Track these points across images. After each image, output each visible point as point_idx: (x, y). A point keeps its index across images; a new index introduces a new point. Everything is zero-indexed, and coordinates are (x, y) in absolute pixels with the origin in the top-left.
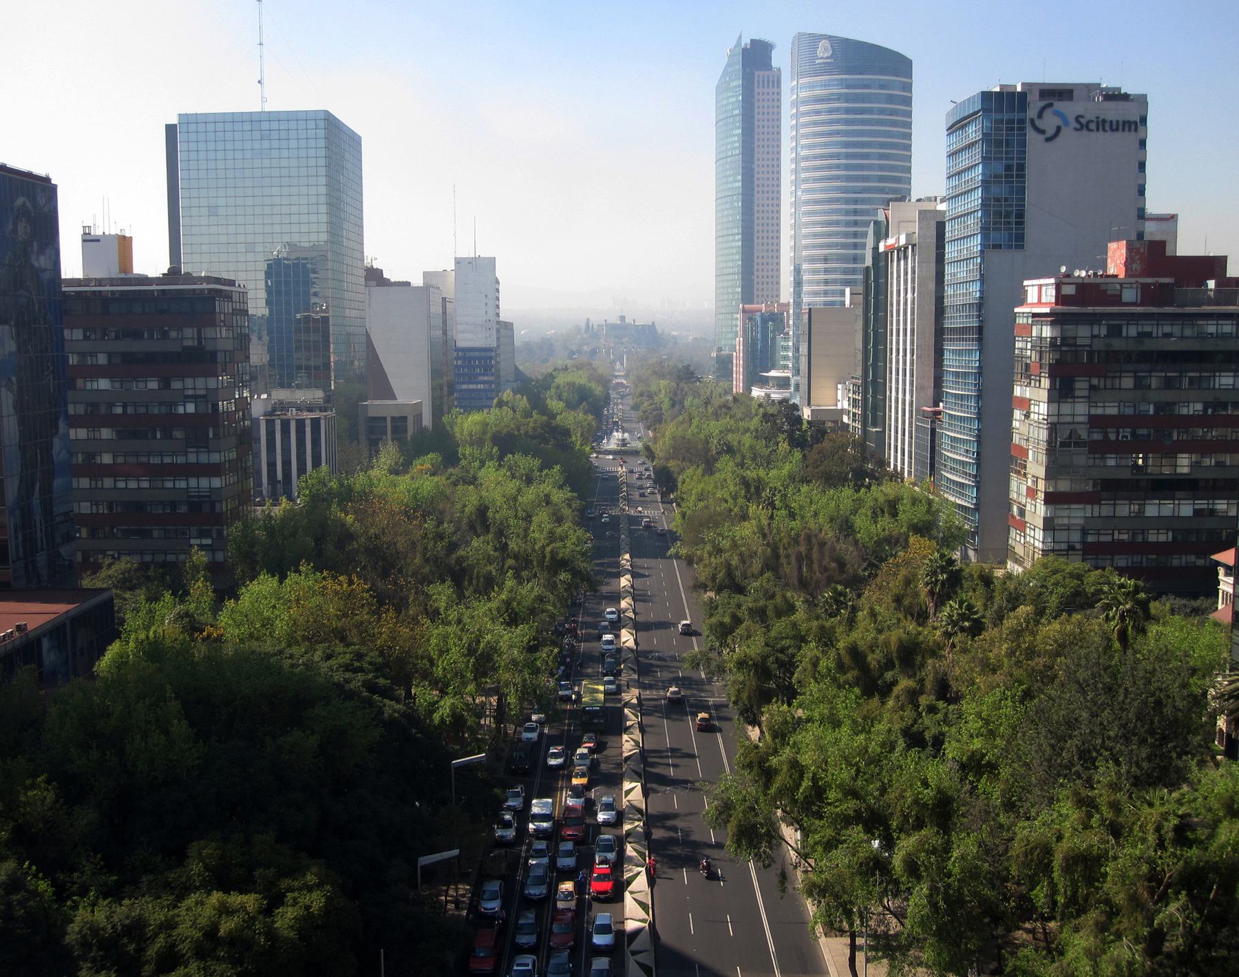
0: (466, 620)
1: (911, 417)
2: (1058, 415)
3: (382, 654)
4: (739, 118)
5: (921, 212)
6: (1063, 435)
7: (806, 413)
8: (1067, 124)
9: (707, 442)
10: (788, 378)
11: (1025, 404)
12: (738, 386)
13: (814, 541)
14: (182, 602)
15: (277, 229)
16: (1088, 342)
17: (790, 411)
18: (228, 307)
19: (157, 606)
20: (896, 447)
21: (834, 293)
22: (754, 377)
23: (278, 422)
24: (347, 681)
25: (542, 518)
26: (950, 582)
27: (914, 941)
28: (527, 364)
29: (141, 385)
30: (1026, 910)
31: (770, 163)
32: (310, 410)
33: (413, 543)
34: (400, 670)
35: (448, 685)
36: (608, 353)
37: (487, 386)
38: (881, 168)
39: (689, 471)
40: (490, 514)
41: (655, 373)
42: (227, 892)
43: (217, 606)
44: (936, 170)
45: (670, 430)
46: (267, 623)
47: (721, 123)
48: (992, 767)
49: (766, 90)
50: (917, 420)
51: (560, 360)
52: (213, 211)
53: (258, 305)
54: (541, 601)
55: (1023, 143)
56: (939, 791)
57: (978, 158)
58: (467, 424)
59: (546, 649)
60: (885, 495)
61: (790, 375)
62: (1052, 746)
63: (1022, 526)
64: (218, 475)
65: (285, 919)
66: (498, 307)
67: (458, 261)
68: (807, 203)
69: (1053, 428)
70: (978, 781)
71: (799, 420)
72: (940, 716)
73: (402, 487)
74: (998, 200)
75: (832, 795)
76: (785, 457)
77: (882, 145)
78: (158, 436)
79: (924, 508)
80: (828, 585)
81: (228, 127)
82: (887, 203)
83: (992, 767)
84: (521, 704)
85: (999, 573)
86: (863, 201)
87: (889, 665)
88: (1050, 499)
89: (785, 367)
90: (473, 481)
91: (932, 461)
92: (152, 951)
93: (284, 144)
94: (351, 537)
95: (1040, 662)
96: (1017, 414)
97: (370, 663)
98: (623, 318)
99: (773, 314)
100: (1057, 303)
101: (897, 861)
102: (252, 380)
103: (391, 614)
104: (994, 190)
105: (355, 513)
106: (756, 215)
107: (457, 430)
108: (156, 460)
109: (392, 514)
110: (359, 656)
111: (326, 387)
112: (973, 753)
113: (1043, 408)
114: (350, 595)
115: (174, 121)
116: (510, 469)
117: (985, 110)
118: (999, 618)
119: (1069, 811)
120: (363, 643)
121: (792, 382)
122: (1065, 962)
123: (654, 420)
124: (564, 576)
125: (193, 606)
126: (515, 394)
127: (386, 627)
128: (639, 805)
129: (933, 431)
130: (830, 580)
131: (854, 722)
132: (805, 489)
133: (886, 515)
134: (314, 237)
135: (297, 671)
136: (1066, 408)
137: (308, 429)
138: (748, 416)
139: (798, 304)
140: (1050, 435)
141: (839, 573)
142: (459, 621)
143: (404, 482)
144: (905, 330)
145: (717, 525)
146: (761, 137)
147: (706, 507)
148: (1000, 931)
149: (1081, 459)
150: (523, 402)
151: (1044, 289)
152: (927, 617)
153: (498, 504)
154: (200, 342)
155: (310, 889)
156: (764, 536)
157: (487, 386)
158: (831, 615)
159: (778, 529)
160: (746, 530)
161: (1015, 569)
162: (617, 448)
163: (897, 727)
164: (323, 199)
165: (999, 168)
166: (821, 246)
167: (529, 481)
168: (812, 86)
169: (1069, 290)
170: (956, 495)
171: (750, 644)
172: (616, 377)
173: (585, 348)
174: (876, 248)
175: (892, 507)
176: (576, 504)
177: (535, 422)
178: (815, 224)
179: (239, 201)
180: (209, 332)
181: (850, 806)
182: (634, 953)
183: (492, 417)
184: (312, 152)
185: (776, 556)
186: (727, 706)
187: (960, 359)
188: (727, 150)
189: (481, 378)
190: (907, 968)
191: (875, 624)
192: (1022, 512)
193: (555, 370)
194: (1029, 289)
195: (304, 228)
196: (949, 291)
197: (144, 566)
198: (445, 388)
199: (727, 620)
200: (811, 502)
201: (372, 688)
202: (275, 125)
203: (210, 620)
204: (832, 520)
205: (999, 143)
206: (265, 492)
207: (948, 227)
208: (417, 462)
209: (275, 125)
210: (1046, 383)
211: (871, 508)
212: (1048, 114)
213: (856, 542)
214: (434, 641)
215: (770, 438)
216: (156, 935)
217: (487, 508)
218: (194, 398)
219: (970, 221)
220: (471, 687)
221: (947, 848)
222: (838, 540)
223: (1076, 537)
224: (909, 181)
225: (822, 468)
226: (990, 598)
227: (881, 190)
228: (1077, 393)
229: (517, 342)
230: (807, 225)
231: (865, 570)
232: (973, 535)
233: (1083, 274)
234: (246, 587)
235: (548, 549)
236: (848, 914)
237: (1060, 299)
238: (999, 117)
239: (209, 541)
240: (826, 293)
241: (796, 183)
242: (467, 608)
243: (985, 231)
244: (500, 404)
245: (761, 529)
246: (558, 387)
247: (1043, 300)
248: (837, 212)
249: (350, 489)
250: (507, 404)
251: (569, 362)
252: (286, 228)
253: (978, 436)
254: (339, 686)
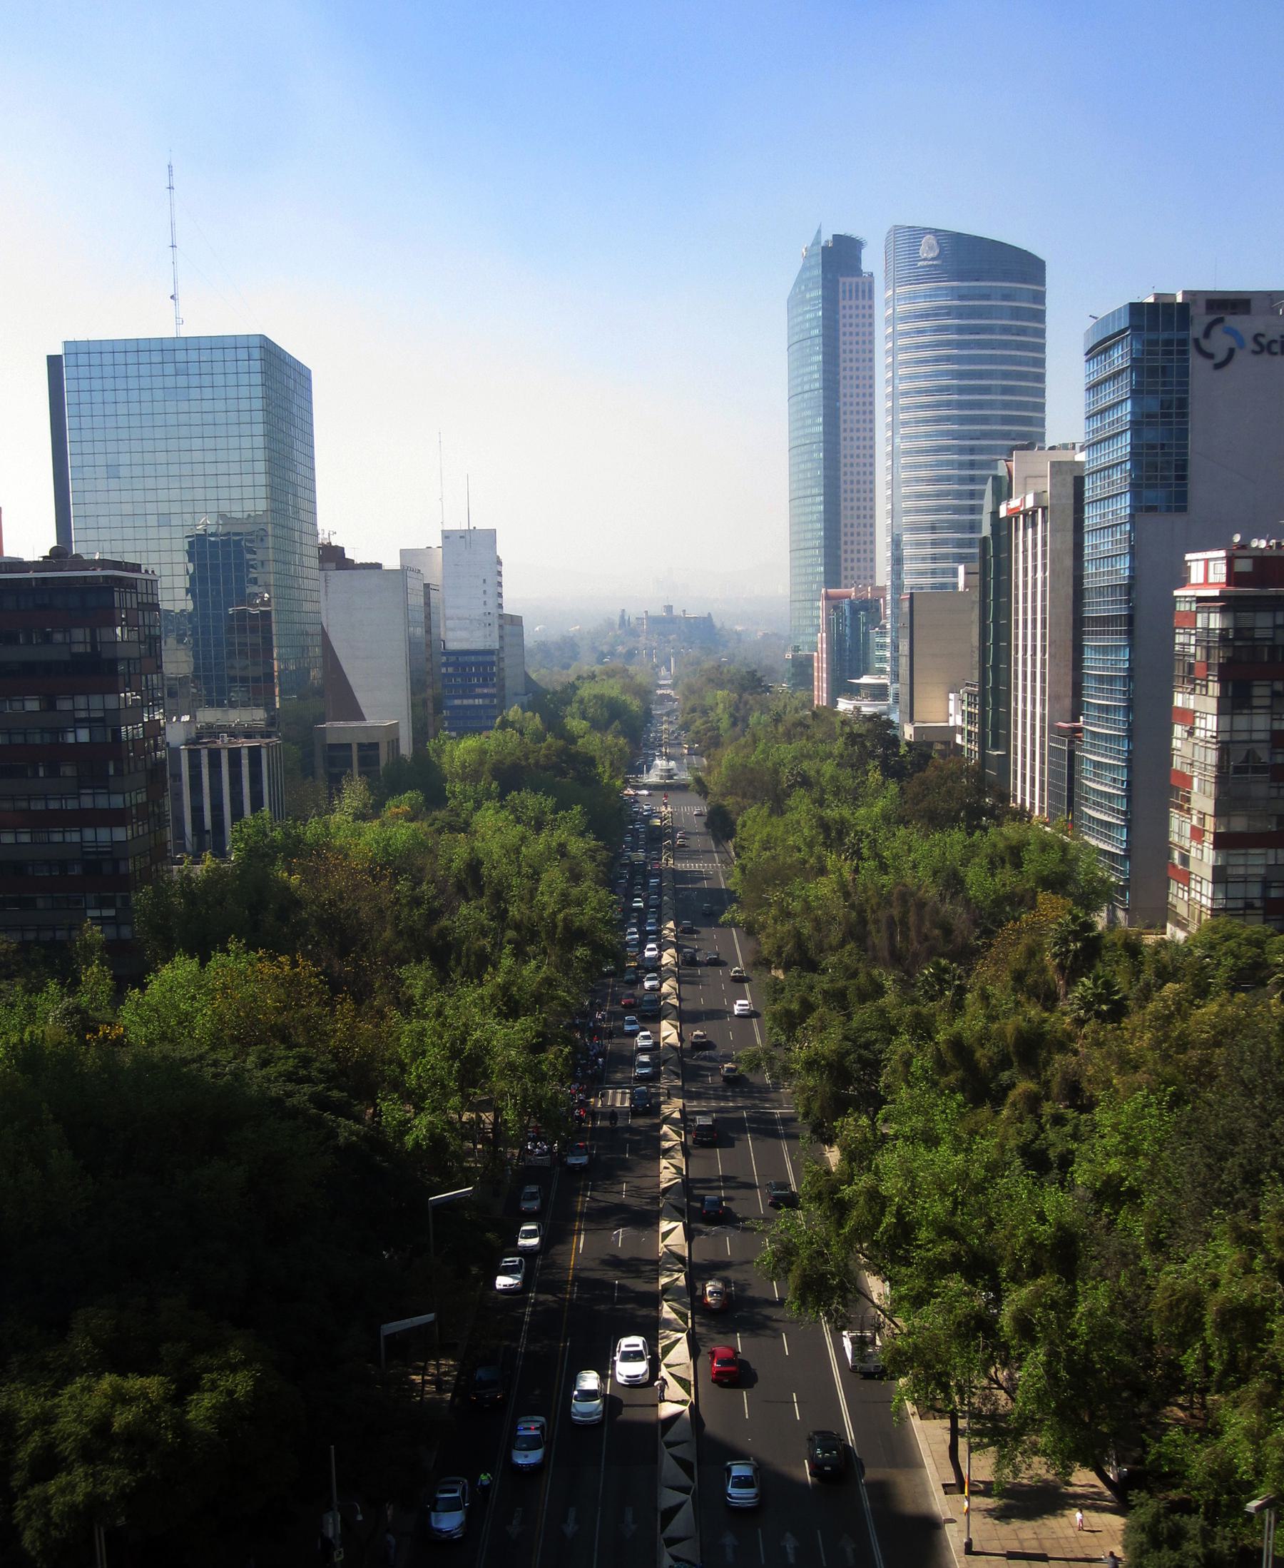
0: (448, 1011)
1: (1042, 736)
2: (1231, 731)
3: (336, 1057)
4: (819, 340)
5: (1053, 464)
6: (1237, 758)
7: (908, 732)
8: (1242, 345)
9: (776, 772)
10: (884, 686)
11: (1188, 717)
12: (821, 696)
13: (911, 901)
14: (72, 992)
15: (199, 494)
16: (1269, 634)
17: (881, 728)
18: (131, 600)
19: (38, 1000)
20: (1024, 776)
21: (944, 572)
22: (841, 686)
23: (204, 753)
24: (289, 1095)
25: (554, 875)
26: (1086, 952)
27: (1027, 1423)
28: (543, 671)
29: (17, 705)
30: (1174, 1381)
32: (248, 735)
33: (381, 911)
34: (361, 1079)
35: (424, 1098)
36: (650, 655)
37: (487, 702)
38: (1006, 405)
39: (752, 811)
40: (484, 871)
41: (710, 680)
42: (123, 1374)
43: (118, 998)
44: (1073, 407)
45: (727, 755)
46: (186, 1019)
47: (796, 347)
48: (1134, 1194)
49: (853, 303)
50: (1051, 740)
51: (586, 664)
52: (112, 471)
53: (174, 594)
54: (550, 985)
55: (1184, 372)
56: (1060, 1227)
57: (1125, 392)
58: (460, 750)
59: (554, 1049)
60: (1006, 839)
61: (887, 681)
62: (1208, 1166)
63: (1185, 878)
64: (122, 824)
65: (201, 1407)
66: (500, 595)
67: (447, 535)
68: (908, 453)
69: (1225, 749)
70: (1117, 1213)
71: (895, 741)
72: (1068, 1129)
73: (369, 837)
74: (1153, 447)
75: (923, 1234)
76: (876, 791)
77: (1006, 375)
78: (41, 774)
79: (1055, 855)
80: (928, 959)
81: (95, 359)
82: (1011, 450)
83: (1134, 1194)
84: (521, 1120)
85: (1150, 939)
86: (981, 450)
87: (1004, 1062)
88: (1221, 842)
89: (882, 671)
90: (465, 828)
91: (1068, 791)
92: (23, 1455)
93: (206, 380)
94: (298, 904)
95: (1194, 1055)
96: (1179, 730)
97: (321, 1071)
98: (669, 608)
99: (866, 601)
100: (1228, 583)
101: (1006, 1321)
102: (172, 696)
103: (349, 1005)
104: (1150, 435)
105: (304, 872)
106: (843, 470)
107: (445, 759)
108: (38, 806)
109: (353, 873)
110: (306, 1061)
111: (269, 706)
112: (1109, 1176)
113: (1211, 723)
114: (294, 981)
115: (59, 351)
116: (514, 810)
117: (1135, 327)
118: (1146, 996)
119: (1228, 1252)
120: (311, 1044)
121: (891, 691)
122: (1219, 1446)
123: (710, 742)
124: (581, 952)
125: (86, 998)
126: (524, 711)
127: (342, 1023)
128: (680, 1252)
129: (1071, 755)
130: (931, 952)
131: (957, 1138)
132: (902, 832)
133: (1008, 866)
134: (249, 505)
135: (221, 1083)
136: (1241, 722)
137: (245, 762)
138: (831, 737)
139: (897, 587)
140: (1220, 758)
141: (931, 940)
142: (439, 1014)
143: (371, 830)
144: (1034, 620)
145: (785, 881)
146: (848, 364)
147: (774, 858)
148: (1143, 1407)
149: (1260, 788)
150: (535, 722)
151: (1211, 564)
152: (1057, 999)
153: (495, 857)
154: (94, 647)
155: (234, 1369)
156: (847, 895)
157: (487, 702)
158: (932, 999)
159: (865, 885)
160: (824, 888)
161: (1174, 933)
162: (662, 783)
163: (1012, 1143)
164: (260, 454)
165: (1153, 404)
166: (928, 511)
167: (539, 827)
168: (913, 297)
169: (1243, 566)
170: (1102, 837)
171: (825, 1039)
172: (661, 687)
173: (620, 649)
174: (995, 513)
175: (1015, 855)
176: (602, 856)
177: (549, 748)
178: (918, 480)
179: (148, 457)
180: (104, 634)
181: (946, 1248)
182: (669, 1445)
183: (492, 742)
184: (244, 392)
185: (863, 921)
186: (795, 1120)
187: (1106, 658)
188: (803, 384)
189: (478, 691)
190: (1019, 1459)
191: (988, 1009)
192: (1185, 859)
193: (579, 678)
194: (1193, 565)
195: (236, 493)
196: (1089, 569)
197: (24, 946)
198: (430, 705)
199: (795, 1006)
200: (910, 850)
201: (322, 1103)
202: (193, 356)
203: (109, 1017)
204: (935, 873)
205: (1152, 372)
206: (188, 845)
207: (1088, 484)
208: (390, 803)
209: (218, 355)
210: (1214, 688)
211: (987, 856)
212: (1217, 332)
213: (968, 901)
214: (405, 1040)
215: (858, 765)
216: (29, 1433)
217: (480, 863)
218: (89, 722)
219: (1116, 475)
220: (455, 1100)
221: (1071, 1302)
222: (943, 900)
223: (1255, 891)
224: (1041, 422)
225: (924, 805)
226: (1137, 973)
227: (1006, 435)
228: (1256, 702)
229: (529, 641)
230: (908, 482)
231: (978, 938)
232: (1122, 891)
233: (1263, 544)
234: (156, 972)
235: (561, 916)
236: (945, 1388)
237: (1233, 577)
238: (1153, 336)
239: (111, 913)
240: (934, 573)
241: (893, 427)
242: (450, 996)
243: (1136, 488)
244: (505, 725)
245: (843, 886)
246: (581, 701)
247: (1211, 580)
248: (949, 463)
249: (299, 840)
250: (512, 725)
251: (597, 668)
252: (211, 494)
253: (1128, 760)
254: (278, 1101)
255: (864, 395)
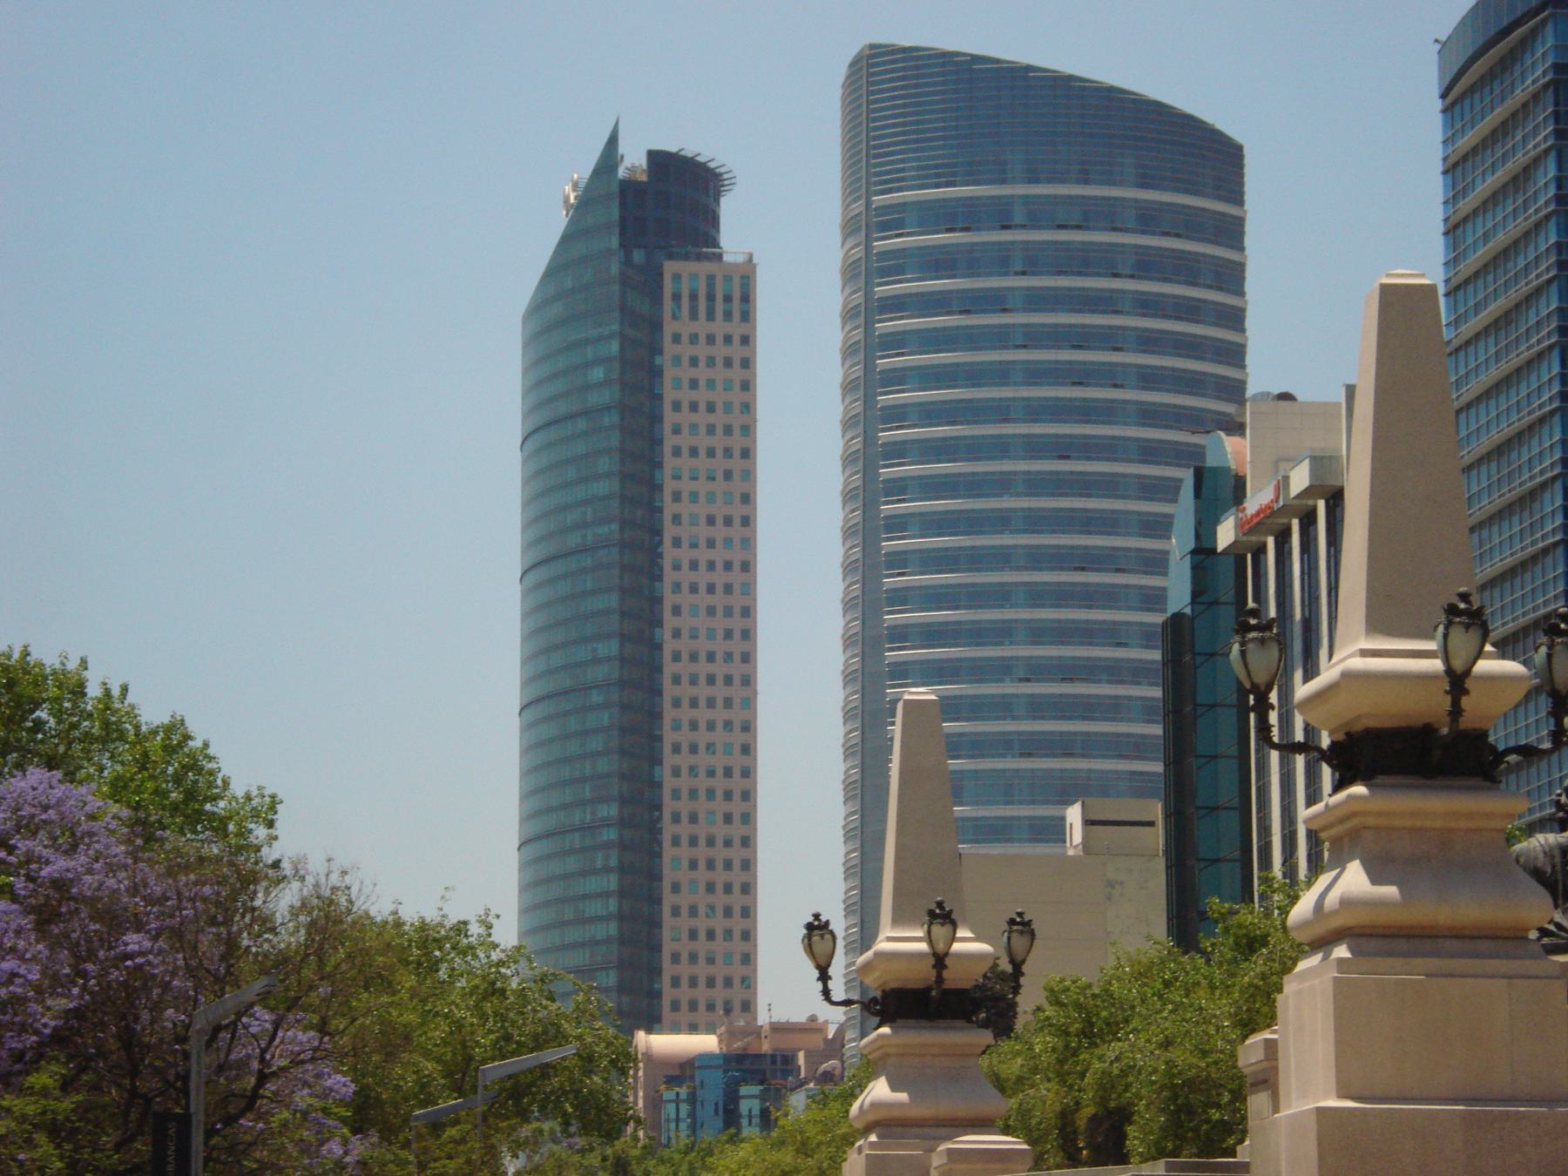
31: (720, 783)
49: (702, 327)
174: (1203, 552)
255: (728, 772)
